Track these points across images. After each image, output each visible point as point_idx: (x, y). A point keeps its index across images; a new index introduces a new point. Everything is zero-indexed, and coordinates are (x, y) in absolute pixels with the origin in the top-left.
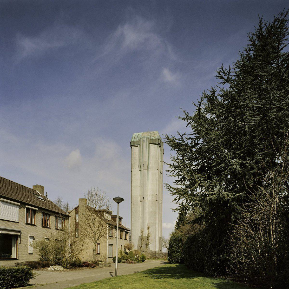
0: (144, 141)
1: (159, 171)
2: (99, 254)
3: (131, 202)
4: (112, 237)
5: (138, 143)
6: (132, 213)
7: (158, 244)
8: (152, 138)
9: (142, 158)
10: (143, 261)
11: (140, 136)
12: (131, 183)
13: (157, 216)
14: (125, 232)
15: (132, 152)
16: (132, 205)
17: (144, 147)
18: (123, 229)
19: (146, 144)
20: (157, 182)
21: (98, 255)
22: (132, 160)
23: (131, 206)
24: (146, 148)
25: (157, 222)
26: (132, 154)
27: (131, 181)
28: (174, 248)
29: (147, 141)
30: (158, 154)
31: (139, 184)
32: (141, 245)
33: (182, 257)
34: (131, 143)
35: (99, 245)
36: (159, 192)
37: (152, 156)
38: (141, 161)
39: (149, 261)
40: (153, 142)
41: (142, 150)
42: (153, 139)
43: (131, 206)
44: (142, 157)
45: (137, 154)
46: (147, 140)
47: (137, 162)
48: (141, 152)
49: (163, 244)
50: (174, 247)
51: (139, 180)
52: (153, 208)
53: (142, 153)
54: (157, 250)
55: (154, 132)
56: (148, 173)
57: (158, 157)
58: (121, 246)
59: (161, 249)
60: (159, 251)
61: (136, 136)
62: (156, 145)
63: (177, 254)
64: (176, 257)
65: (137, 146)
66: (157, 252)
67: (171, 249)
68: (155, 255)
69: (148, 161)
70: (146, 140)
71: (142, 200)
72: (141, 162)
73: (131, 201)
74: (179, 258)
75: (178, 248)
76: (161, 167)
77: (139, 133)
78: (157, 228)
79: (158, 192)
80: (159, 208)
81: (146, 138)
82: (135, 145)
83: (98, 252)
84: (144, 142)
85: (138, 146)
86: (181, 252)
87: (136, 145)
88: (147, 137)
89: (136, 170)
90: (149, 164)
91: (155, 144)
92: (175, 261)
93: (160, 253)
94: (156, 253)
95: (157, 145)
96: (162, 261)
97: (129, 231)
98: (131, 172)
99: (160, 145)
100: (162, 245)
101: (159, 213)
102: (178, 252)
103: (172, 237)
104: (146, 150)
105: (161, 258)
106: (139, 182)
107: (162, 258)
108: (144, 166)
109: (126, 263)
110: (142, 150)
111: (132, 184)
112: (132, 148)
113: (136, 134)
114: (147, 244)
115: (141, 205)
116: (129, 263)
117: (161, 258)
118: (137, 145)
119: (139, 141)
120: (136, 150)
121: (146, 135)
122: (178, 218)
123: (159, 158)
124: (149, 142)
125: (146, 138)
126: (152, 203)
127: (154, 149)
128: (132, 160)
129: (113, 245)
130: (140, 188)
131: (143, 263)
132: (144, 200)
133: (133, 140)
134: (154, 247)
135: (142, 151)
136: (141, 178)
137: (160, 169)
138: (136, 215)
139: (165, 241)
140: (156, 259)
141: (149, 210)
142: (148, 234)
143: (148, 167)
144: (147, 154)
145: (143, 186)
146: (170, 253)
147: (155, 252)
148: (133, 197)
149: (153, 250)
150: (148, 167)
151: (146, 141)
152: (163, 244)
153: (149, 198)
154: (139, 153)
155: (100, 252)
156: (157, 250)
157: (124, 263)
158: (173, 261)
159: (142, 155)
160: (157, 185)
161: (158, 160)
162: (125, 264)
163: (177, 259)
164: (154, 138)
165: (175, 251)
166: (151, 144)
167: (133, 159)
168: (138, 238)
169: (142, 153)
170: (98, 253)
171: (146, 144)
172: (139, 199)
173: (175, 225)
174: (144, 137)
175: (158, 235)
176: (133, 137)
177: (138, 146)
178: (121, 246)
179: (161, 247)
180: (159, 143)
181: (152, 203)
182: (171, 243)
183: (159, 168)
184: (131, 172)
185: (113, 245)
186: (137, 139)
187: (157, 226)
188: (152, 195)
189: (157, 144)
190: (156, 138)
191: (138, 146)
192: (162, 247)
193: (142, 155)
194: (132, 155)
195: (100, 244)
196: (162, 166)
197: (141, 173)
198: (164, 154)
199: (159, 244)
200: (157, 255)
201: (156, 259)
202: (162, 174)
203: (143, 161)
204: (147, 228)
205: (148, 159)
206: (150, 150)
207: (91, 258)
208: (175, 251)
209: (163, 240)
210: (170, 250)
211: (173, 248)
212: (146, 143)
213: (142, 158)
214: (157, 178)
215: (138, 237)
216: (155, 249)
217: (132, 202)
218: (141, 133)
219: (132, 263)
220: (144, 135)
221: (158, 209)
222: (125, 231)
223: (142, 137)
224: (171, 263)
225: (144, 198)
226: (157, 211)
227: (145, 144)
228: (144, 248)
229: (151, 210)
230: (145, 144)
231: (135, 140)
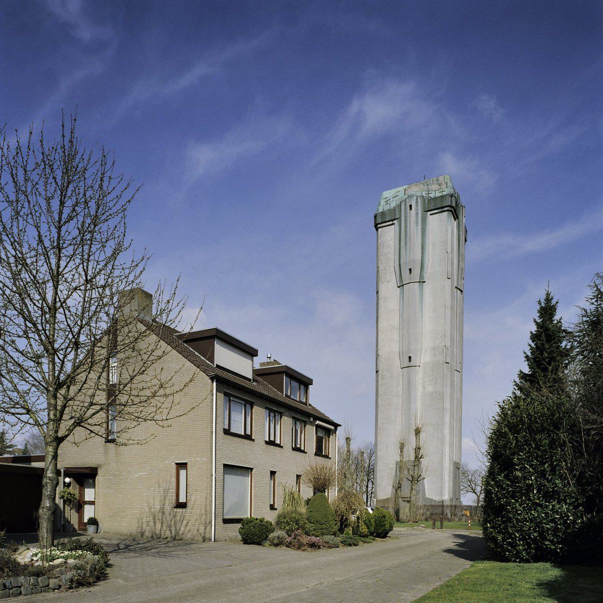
0: (411, 206)
1: (452, 282)
2: (183, 506)
3: (377, 372)
4: (248, 437)
5: (395, 215)
6: (379, 401)
7: (450, 480)
8: (432, 195)
9: (406, 253)
10: (383, 535)
11: (401, 194)
12: (377, 323)
13: (447, 405)
14: (318, 426)
15: (378, 241)
16: (380, 378)
17: (412, 221)
18: (308, 415)
19: (417, 213)
20: (448, 312)
21: (181, 510)
22: (378, 261)
23: (377, 381)
24: (417, 223)
25: (447, 419)
26: (377, 245)
27: (377, 318)
28: (525, 471)
29: (419, 205)
30: (449, 237)
31: (396, 322)
32: (399, 483)
33: (574, 522)
34: (375, 217)
35: (186, 471)
36: (452, 339)
37: (433, 244)
38: (402, 259)
39: (413, 532)
40: (435, 206)
41: (406, 231)
42: (435, 198)
43: (377, 381)
44: (406, 249)
45: (392, 243)
46: (419, 203)
47: (392, 264)
48: (402, 240)
49: (464, 484)
50: (523, 469)
51: (397, 313)
52: (436, 383)
53: (406, 239)
54: (446, 497)
55: (437, 180)
56: (421, 289)
57: (449, 244)
58: (273, 473)
59: (460, 496)
60: (451, 500)
61: (390, 197)
62: (443, 213)
63: (541, 506)
64: (538, 524)
65: (391, 223)
66: (445, 504)
67: (506, 477)
68: (440, 511)
69: (422, 258)
70: (417, 202)
71: (407, 363)
72: (402, 262)
73: (376, 369)
74: (555, 530)
75: (553, 470)
76: (460, 272)
77: (398, 189)
78: (447, 438)
79: (449, 340)
80: (452, 382)
81: (415, 198)
82: (386, 222)
83: (182, 499)
84: (411, 209)
85: (394, 224)
86: (569, 495)
87: (389, 221)
88: (419, 194)
89: (389, 287)
90: (426, 265)
91: (441, 209)
92: (529, 545)
93: (455, 506)
94: (443, 506)
95: (446, 213)
96: (456, 533)
97: (336, 426)
98: (377, 292)
99: (454, 209)
100: (462, 487)
101: (452, 394)
102: (550, 496)
103: (504, 414)
104: (417, 229)
105: (457, 519)
106: (397, 317)
107: (460, 520)
108: (411, 273)
109: (287, 546)
110: (406, 231)
111: (379, 322)
112: (379, 230)
113: (387, 194)
114: (415, 480)
115: (401, 377)
116: (299, 548)
117: (457, 519)
118: (392, 220)
119: (397, 208)
120: (389, 234)
121: (417, 190)
122: (527, 357)
123: (452, 247)
124: (424, 207)
125: (417, 199)
126: (432, 371)
127: (440, 223)
128: (379, 262)
129: (252, 469)
130: (401, 334)
131: (378, 544)
132: (411, 364)
133: (381, 210)
134: (437, 488)
135: (406, 235)
136: (401, 308)
137: (455, 277)
138: (389, 405)
139: (470, 477)
140: (438, 524)
141: (424, 388)
142: (418, 449)
143: (421, 276)
144: (420, 240)
145: (408, 324)
146: (499, 499)
147: (441, 504)
148: (380, 359)
149: (436, 498)
150: (421, 276)
151: (417, 206)
152: (464, 484)
153: (424, 358)
154: (398, 239)
155: (188, 498)
156: (446, 497)
157: (276, 545)
158: (513, 545)
159: (406, 244)
160: (448, 321)
161: (449, 251)
162: (283, 551)
163: (541, 534)
164: (438, 194)
165: (530, 488)
166: (429, 213)
167: (381, 258)
168: (394, 463)
169: (406, 239)
170: (181, 501)
171: (417, 213)
172: (397, 363)
173: (516, 385)
174: (411, 196)
175: (451, 458)
176: (383, 202)
177: (394, 224)
178: (273, 473)
179: (460, 490)
180: (454, 205)
181: (432, 371)
182: (505, 446)
183: (452, 273)
184: (377, 292)
185: (252, 469)
186: (393, 205)
187: (447, 432)
188: (434, 347)
189: (446, 209)
190: (444, 193)
191: (394, 222)
192: (462, 492)
193: (406, 244)
194: (378, 249)
195: (186, 464)
196: (460, 270)
197: (402, 293)
198: (466, 241)
199: (453, 482)
200: (448, 512)
201: (438, 524)
202: (462, 291)
203: (408, 260)
204: (413, 433)
205: (422, 253)
206: (426, 229)
207: (155, 523)
208: (530, 488)
209: (463, 473)
210: (498, 485)
211: (519, 474)
212: (417, 210)
213: (406, 253)
214: (448, 303)
215: (395, 463)
216: (442, 494)
217: (380, 372)
218: (401, 189)
219: (313, 546)
220: (410, 192)
221: (449, 384)
222: (318, 422)
223: (406, 196)
224: (507, 560)
225: (410, 357)
226: (448, 390)
227: (414, 216)
228: (405, 491)
229: (430, 389)
230: (414, 216)
231: (387, 208)
